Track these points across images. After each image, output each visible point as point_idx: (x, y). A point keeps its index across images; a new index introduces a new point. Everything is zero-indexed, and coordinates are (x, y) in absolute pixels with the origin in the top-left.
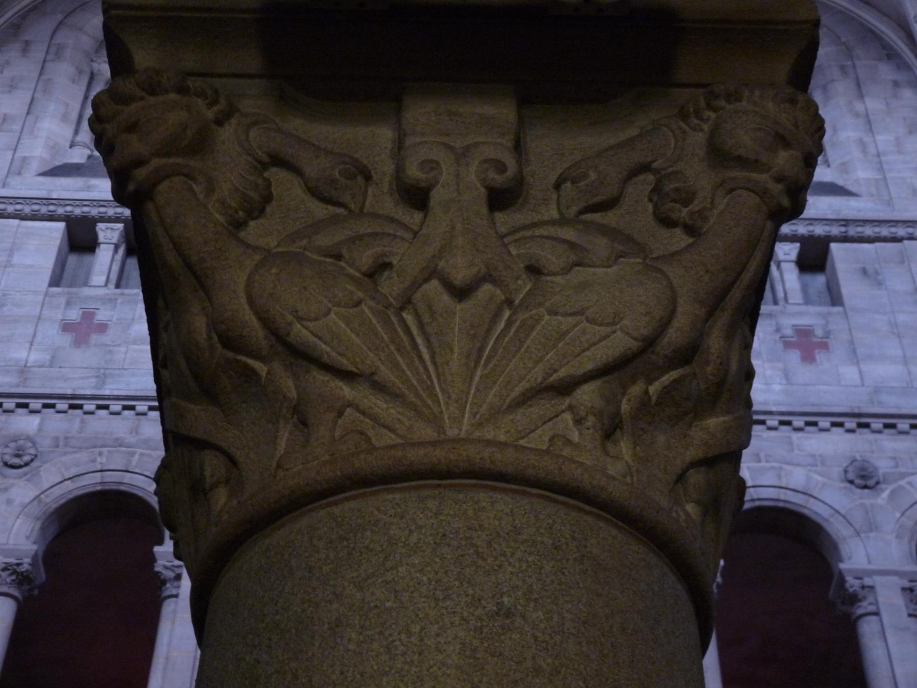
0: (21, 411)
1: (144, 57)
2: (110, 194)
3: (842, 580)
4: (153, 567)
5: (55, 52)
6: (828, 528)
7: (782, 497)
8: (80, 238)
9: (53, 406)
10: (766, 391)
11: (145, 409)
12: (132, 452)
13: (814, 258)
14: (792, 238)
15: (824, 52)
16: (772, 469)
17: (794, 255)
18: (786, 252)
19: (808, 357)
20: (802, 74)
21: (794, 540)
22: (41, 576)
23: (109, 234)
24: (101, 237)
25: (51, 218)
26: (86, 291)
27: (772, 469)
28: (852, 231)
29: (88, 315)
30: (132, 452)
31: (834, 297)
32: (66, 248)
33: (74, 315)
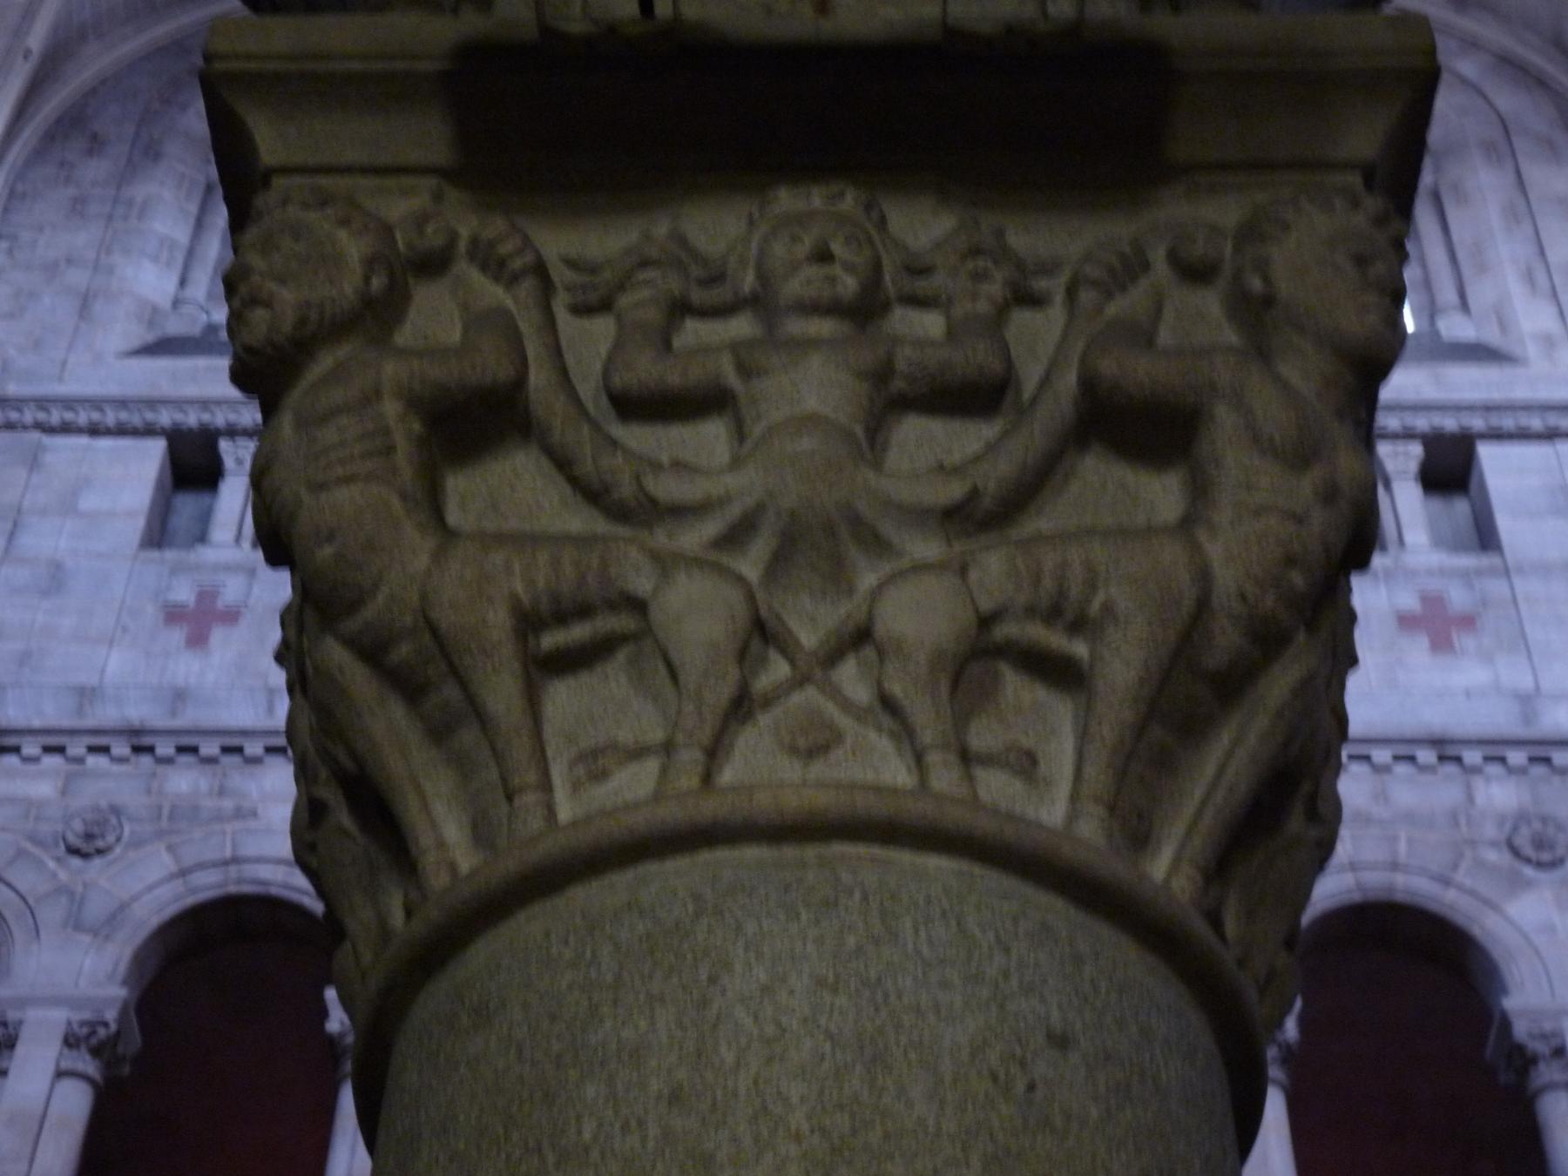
0: (185, 759)
1: (271, 140)
2: (1376, 882)
3: (1506, 1024)
4: (322, 1025)
5: (148, 152)
6: (1476, 931)
7: (167, 389)
8: (192, 465)
9: (193, 750)
10: (1368, 700)
11: (171, 751)
12: (255, 829)
13: (1450, 469)
14: (1408, 435)
15: (1449, 111)
16: (1382, 836)
17: (1413, 466)
18: (1400, 461)
19: (1441, 644)
20: (1397, 179)
21: (1422, 959)
22: (134, 1042)
23: (237, 457)
24: (229, 462)
25: (149, 431)
26: (207, 554)
27: (1382, 836)
28: (1508, 422)
29: (207, 596)
30: (255, 829)
31: (1485, 536)
32: (168, 480)
33: (184, 593)
